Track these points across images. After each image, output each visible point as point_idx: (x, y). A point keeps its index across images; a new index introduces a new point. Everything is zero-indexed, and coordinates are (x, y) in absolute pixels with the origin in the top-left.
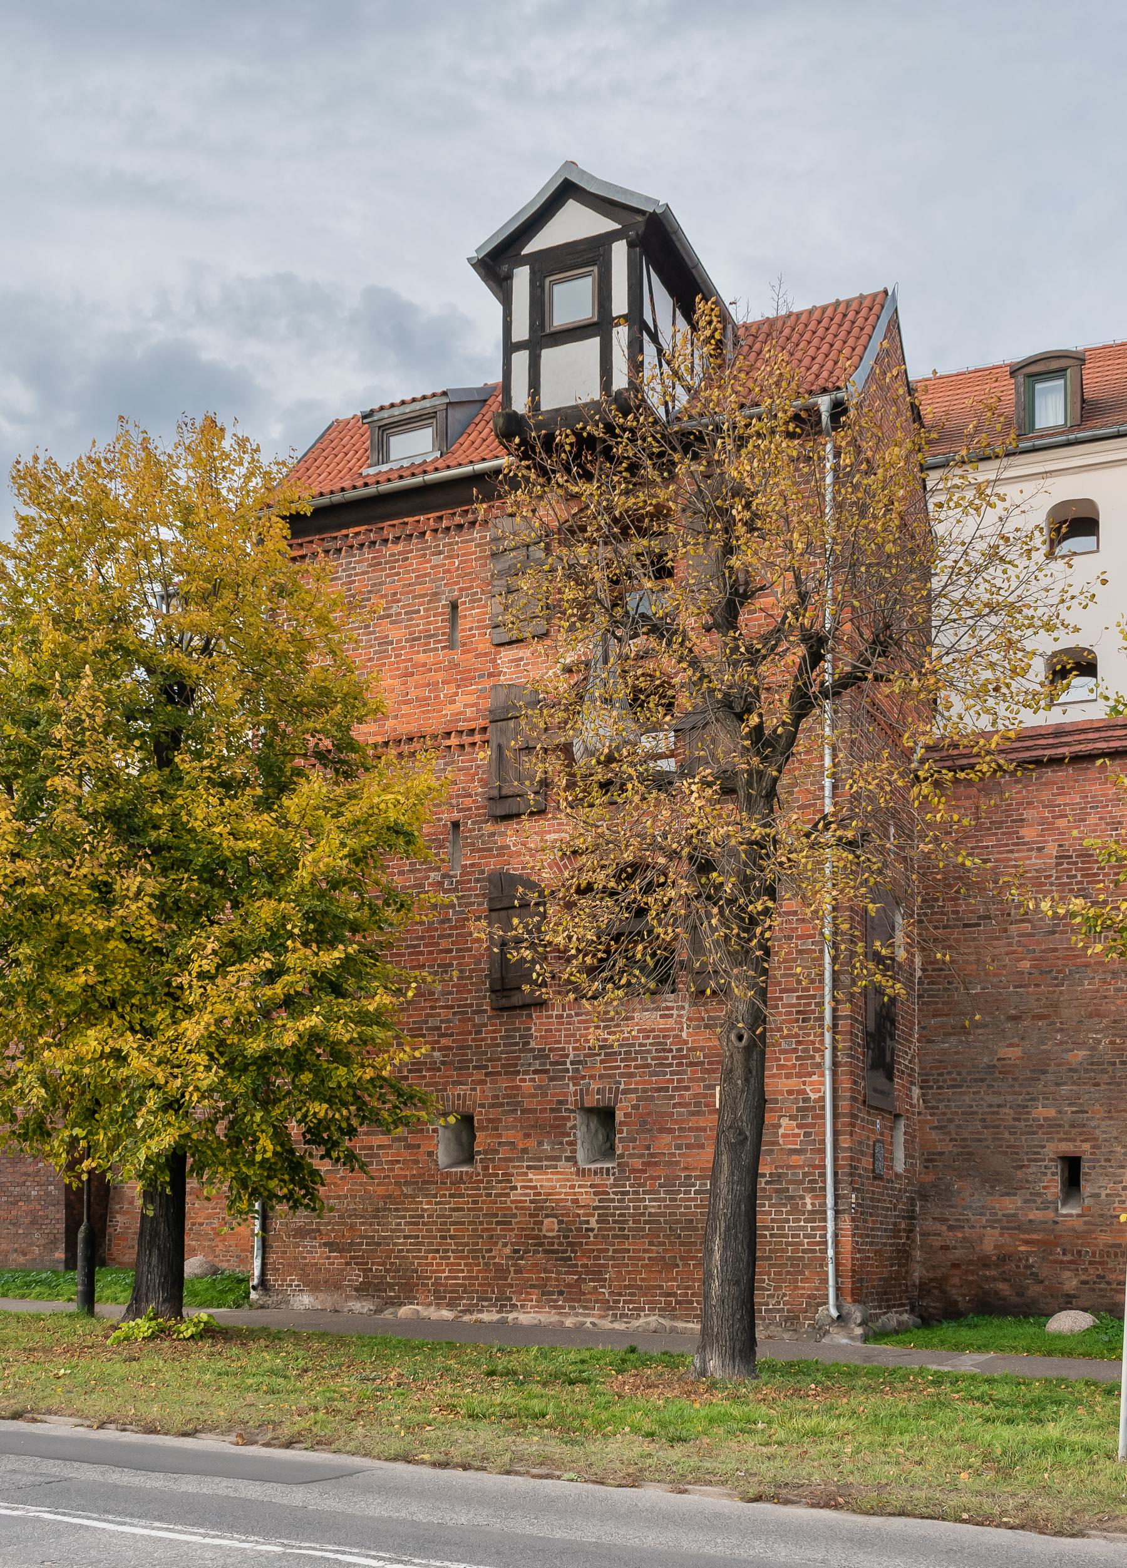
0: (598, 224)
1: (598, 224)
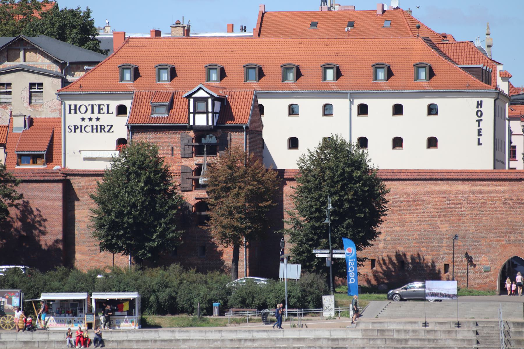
0: (209, 96)
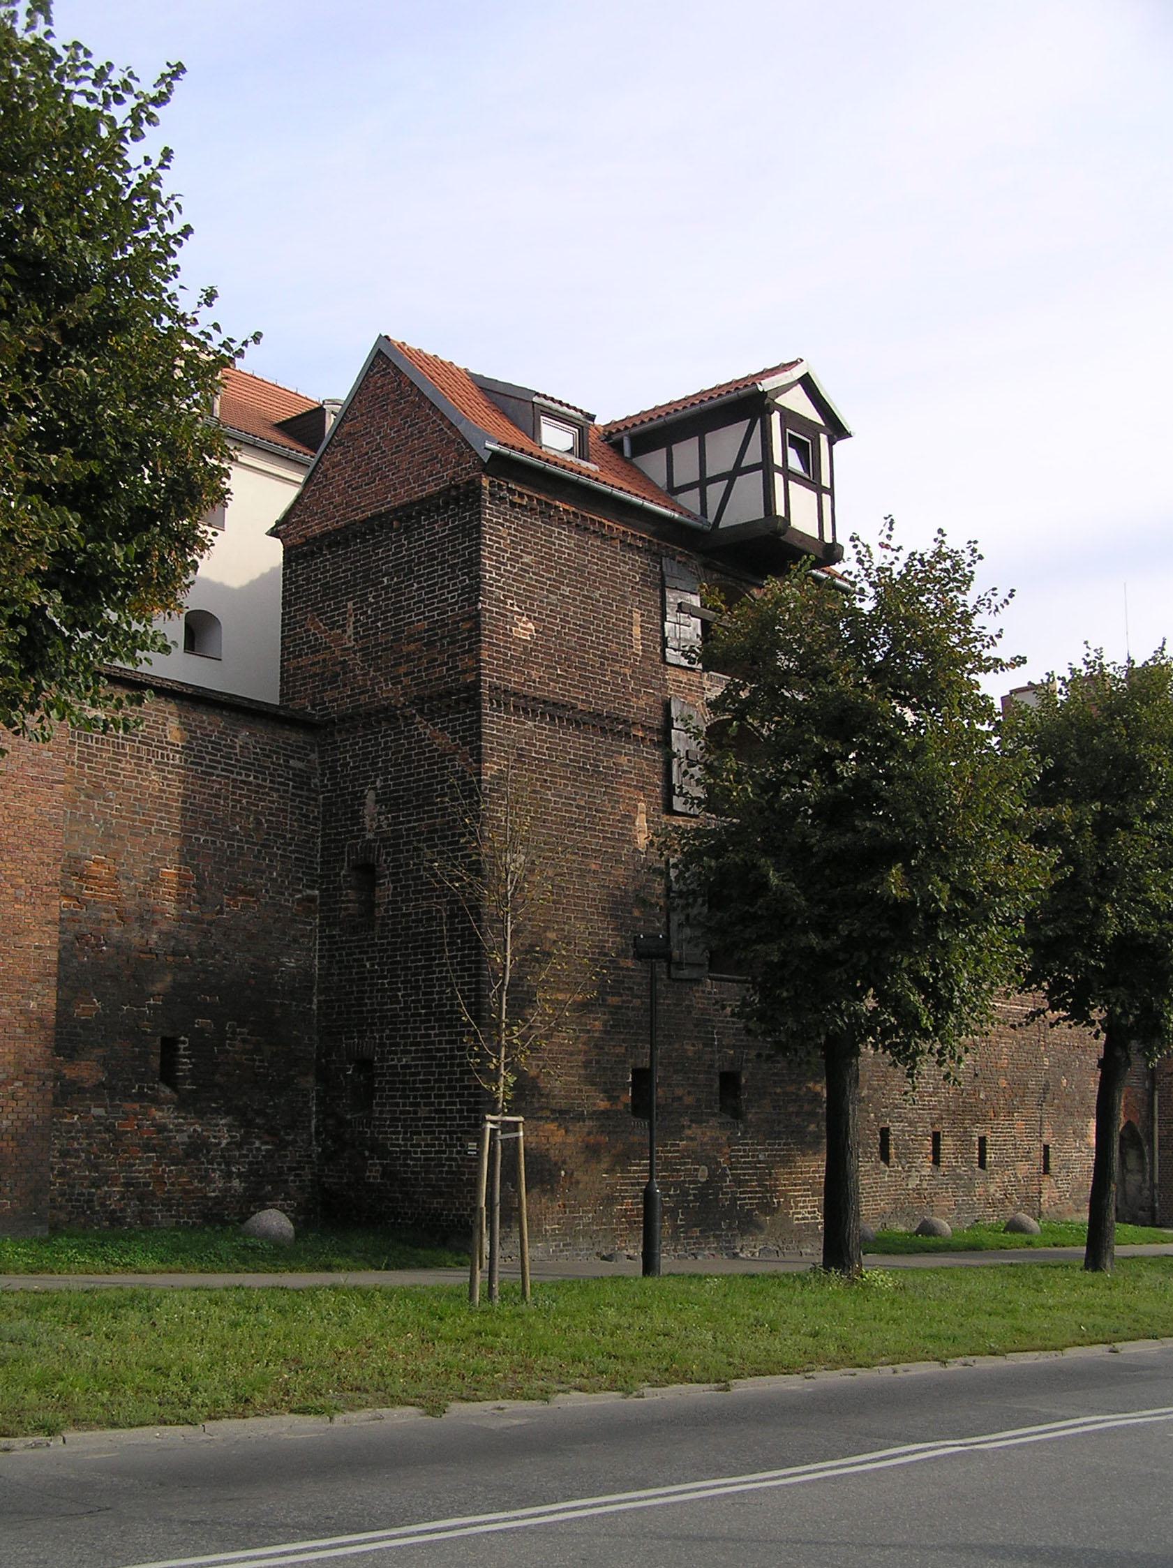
0: (813, 414)
1: (813, 414)
